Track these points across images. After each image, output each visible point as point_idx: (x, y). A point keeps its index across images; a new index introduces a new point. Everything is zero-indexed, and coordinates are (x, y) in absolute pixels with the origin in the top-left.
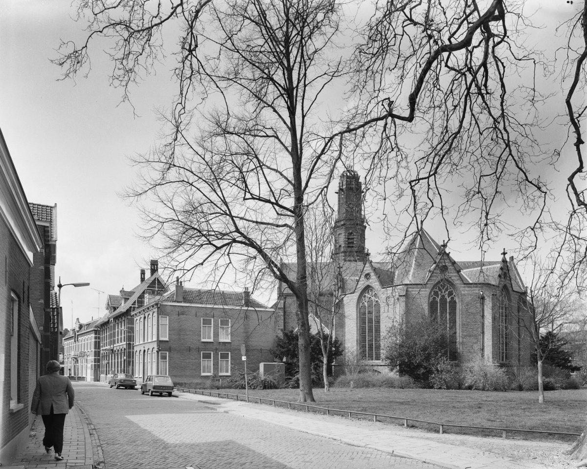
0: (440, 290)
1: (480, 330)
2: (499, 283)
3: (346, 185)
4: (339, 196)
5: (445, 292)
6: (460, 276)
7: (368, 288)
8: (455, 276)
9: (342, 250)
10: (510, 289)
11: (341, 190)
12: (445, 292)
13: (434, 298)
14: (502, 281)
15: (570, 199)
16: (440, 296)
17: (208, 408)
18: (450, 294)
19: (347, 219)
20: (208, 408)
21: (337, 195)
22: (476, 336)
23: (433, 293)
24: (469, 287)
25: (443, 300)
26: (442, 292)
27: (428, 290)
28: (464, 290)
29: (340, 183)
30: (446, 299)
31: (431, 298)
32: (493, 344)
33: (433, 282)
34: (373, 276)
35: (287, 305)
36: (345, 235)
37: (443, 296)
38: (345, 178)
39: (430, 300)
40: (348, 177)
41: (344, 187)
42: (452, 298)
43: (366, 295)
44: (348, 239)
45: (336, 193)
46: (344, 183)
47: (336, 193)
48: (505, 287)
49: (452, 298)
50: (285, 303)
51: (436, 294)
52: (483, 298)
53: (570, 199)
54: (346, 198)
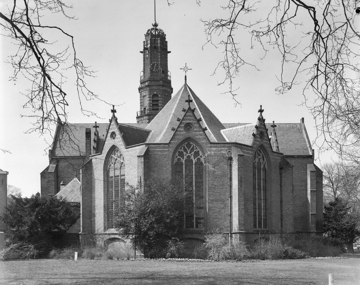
0: (185, 150)
1: (228, 194)
2: (254, 144)
3: (151, 43)
4: (144, 55)
5: (190, 153)
6: (206, 135)
7: (114, 148)
8: (201, 135)
9: (147, 112)
10: (269, 150)
11: (145, 49)
12: (190, 153)
13: (179, 159)
14: (258, 141)
15: (289, 6)
16: (185, 157)
17: (265, 220)
18: (197, 154)
19: (150, 80)
20: (265, 220)
21: (142, 54)
22: (223, 201)
23: (177, 154)
24: (217, 147)
25: (189, 161)
26: (187, 153)
27: (172, 150)
28: (211, 151)
29: (144, 42)
30: (192, 160)
31: (176, 160)
32: (239, 209)
33: (176, 142)
34: (119, 136)
35: (60, 169)
36: (149, 97)
37: (189, 157)
38: (150, 36)
39: (175, 162)
40: (152, 36)
41: (149, 46)
42: (199, 159)
43: (113, 156)
44: (153, 101)
45: (141, 52)
46: (149, 42)
47: (141, 52)
48: (262, 146)
49: (199, 159)
50: (57, 167)
51: (181, 154)
52: (231, 159)
53: (289, 6)
54: (151, 58)
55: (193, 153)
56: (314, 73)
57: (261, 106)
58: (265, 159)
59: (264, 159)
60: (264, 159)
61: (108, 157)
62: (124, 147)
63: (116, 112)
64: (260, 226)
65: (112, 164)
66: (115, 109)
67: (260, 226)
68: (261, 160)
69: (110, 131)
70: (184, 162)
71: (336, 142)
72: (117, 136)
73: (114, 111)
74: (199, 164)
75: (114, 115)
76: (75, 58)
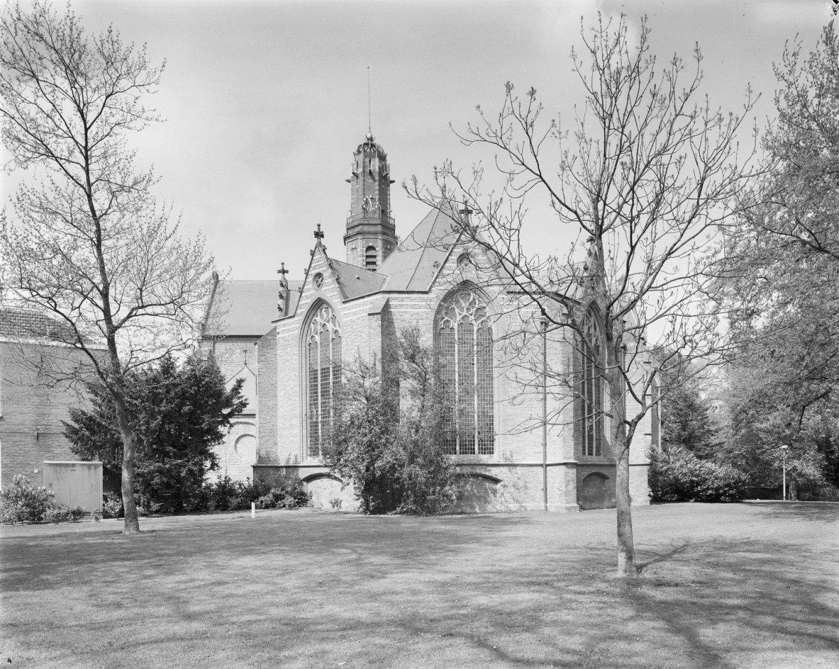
5: (468, 309)
12: (468, 309)
16: (458, 319)
25: (465, 327)
55: (473, 311)
56: (117, 129)
57: (319, 225)
58: (598, 328)
59: (595, 329)
60: (595, 329)
61: (308, 322)
62: (339, 300)
63: (322, 236)
64: (590, 454)
65: (316, 333)
66: (321, 230)
67: (590, 454)
68: (592, 330)
69: (313, 272)
70: (456, 327)
71: (100, 373)
72: (325, 281)
73: (319, 235)
74: (486, 331)
75: (320, 244)
76: (73, 138)
